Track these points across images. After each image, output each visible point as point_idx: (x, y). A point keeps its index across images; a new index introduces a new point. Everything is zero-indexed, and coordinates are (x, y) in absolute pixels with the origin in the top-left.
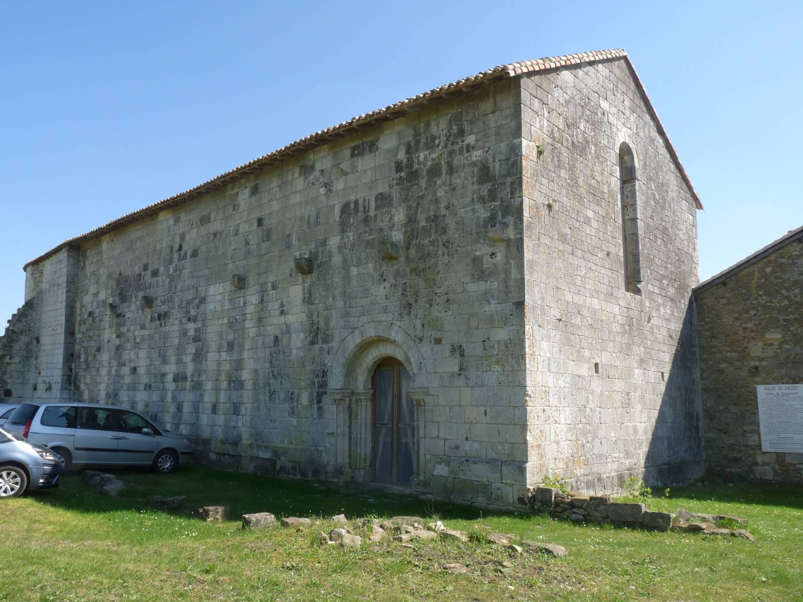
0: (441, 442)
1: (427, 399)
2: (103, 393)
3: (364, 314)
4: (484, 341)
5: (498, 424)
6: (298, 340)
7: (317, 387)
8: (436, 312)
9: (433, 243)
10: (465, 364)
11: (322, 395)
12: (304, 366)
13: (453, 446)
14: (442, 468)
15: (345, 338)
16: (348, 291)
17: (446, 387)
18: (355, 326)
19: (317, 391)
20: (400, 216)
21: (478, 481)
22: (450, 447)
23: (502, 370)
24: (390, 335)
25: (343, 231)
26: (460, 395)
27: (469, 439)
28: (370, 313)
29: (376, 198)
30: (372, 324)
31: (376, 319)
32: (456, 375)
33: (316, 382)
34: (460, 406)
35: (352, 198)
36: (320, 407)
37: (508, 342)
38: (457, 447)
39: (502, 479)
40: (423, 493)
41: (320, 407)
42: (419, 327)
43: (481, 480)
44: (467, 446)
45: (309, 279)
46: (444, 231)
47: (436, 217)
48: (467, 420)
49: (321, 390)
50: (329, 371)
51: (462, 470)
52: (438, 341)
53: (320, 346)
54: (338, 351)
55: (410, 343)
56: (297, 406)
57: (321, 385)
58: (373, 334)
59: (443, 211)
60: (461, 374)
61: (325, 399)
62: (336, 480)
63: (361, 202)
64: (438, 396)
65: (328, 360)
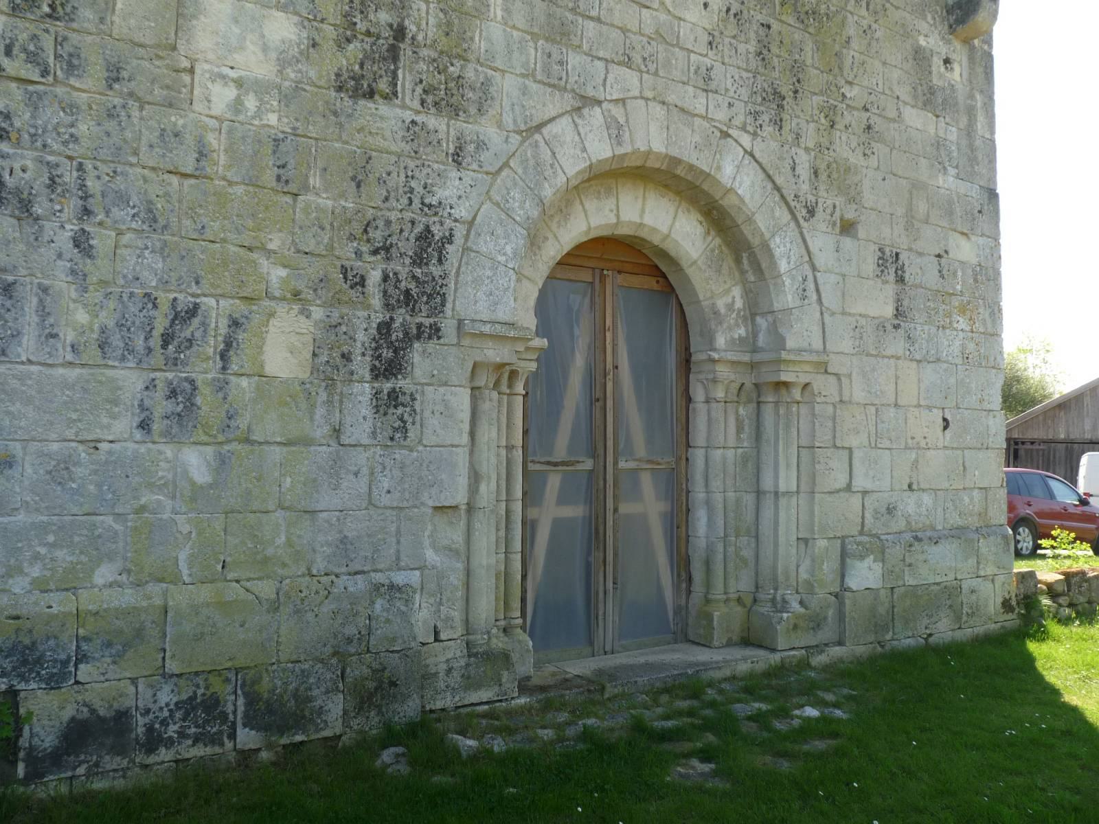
0: (856, 501)
1: (820, 383)
3: (628, 63)
4: (939, 256)
5: (963, 449)
7: (376, 301)
8: (845, 147)
10: (906, 303)
11: (408, 338)
12: (288, 184)
13: (883, 510)
14: (870, 569)
17: (868, 355)
18: (590, 92)
19: (378, 318)
21: (938, 584)
22: (876, 512)
23: (968, 328)
24: (719, 168)
26: (897, 378)
27: (915, 487)
28: (652, 68)
30: (658, 110)
31: (672, 98)
32: (889, 327)
33: (374, 277)
34: (896, 405)
36: (394, 395)
37: (978, 269)
38: (890, 510)
39: (978, 569)
40: (819, 648)
41: (394, 395)
42: (804, 171)
43: (945, 579)
44: (910, 505)
48: (910, 441)
49: (401, 316)
51: (910, 565)
52: (848, 228)
53: (408, 116)
54: (506, 165)
55: (777, 214)
56: (221, 387)
57: (407, 292)
58: (658, 146)
61: (420, 359)
62: (485, 695)
64: (850, 376)
65: (454, 191)
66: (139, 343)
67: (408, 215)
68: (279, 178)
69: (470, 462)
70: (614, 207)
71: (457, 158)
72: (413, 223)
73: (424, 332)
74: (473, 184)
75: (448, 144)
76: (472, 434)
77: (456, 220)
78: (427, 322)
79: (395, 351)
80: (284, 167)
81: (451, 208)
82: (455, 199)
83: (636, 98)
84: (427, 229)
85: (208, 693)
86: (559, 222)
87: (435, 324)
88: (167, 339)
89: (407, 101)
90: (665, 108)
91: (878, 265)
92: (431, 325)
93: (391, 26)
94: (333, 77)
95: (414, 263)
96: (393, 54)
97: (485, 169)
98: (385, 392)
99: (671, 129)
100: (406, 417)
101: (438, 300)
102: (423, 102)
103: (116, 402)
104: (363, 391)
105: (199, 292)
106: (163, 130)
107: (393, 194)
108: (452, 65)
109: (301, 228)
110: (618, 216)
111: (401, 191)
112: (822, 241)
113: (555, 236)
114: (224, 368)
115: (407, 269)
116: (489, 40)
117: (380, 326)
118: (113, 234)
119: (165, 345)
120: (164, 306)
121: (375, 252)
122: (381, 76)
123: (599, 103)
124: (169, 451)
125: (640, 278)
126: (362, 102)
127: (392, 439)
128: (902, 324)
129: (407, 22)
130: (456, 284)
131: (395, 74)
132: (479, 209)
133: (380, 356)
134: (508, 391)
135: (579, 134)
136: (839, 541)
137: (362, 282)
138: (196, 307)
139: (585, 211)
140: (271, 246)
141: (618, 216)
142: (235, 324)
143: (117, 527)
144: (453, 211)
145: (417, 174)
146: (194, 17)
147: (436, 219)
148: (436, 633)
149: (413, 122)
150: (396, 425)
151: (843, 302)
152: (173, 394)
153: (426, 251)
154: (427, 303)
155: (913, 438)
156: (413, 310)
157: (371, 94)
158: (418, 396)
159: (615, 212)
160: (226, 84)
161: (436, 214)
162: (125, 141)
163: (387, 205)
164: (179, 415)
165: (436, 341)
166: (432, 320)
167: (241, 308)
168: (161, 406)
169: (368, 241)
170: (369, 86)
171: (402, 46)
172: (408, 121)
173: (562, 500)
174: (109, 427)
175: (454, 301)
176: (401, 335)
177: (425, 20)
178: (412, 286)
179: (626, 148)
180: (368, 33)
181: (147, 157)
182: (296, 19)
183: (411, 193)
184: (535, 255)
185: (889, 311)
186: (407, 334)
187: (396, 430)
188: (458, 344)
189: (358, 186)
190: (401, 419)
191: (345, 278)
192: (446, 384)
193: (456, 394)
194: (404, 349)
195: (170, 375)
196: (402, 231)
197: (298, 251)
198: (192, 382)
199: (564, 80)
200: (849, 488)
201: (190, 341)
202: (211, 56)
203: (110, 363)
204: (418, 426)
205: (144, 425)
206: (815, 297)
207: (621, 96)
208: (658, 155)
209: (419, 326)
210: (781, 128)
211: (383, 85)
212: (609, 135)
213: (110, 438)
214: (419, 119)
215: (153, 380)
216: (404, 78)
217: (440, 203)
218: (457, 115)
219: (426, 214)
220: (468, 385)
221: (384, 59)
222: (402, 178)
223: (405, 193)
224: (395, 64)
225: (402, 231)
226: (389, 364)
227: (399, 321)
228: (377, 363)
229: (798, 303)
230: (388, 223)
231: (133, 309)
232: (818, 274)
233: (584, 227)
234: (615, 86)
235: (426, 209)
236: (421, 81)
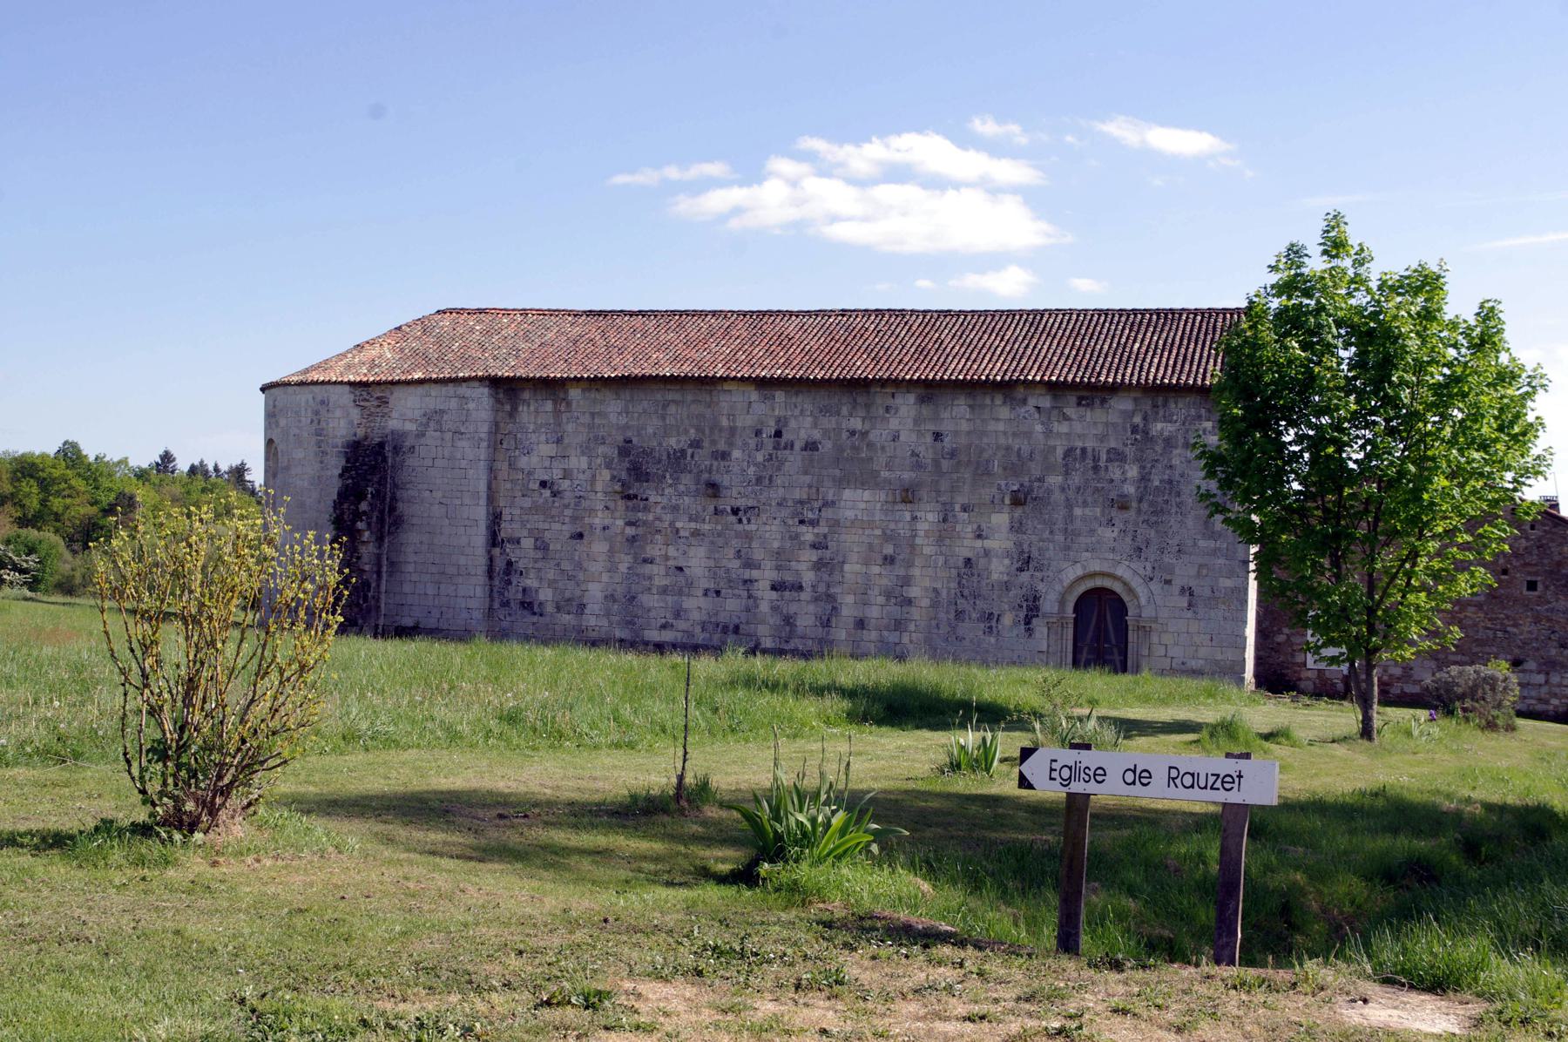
2: (595, 592)
6: (999, 569)
9: (1167, 502)
16: (1070, 528)
20: (1133, 472)
25: (1067, 473)
29: (1108, 452)
35: (1079, 444)
45: (1019, 511)
46: (1179, 494)
47: (1170, 482)
52: (1168, 582)
59: (1177, 477)
61: (1034, 621)
63: (1089, 450)
112: (1155, 586)
226: (1028, 621)
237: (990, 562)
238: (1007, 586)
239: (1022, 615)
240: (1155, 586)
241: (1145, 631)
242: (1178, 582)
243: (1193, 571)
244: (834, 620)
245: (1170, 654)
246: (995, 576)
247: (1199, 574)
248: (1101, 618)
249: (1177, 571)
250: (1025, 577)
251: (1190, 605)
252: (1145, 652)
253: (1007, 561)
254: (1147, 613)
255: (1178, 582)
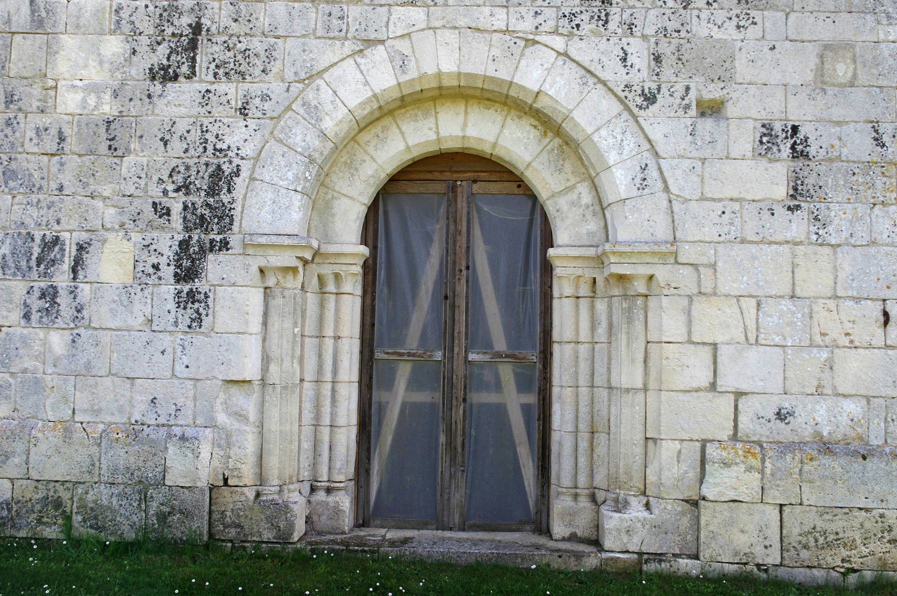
10: (811, 181)
11: (202, 251)
15: (326, 70)
33: (177, 209)
36: (192, 296)
50: (244, 174)
52: (711, 109)
53: (204, 87)
54: (289, 108)
56: (73, 292)
60: (798, 207)
61: (215, 267)
64: (713, 266)
66: (24, 264)
67: (204, 160)
68: (110, 147)
69: (263, 347)
70: (433, 126)
71: (243, 111)
72: (207, 165)
73: (215, 245)
74: (257, 128)
75: (236, 102)
76: (265, 324)
77: (242, 158)
78: (218, 238)
79: (192, 262)
80: (113, 139)
81: (238, 149)
82: (242, 142)
83: (423, 30)
84: (219, 167)
85: (56, 496)
86: (376, 146)
87: (225, 239)
88: (39, 262)
89: (203, 76)
90: (457, 31)
91: (761, 142)
92: (221, 241)
93: (190, 25)
94: (147, 71)
95: (208, 194)
96: (193, 45)
97: (268, 115)
98: (185, 292)
99: (463, 49)
100: (201, 310)
101: (227, 220)
102: (215, 74)
103: (11, 302)
104: (168, 289)
105: (59, 229)
106: (38, 128)
107: (191, 146)
108: (240, 42)
109: (125, 179)
110: (438, 133)
111: (198, 143)
112: (665, 125)
113: (372, 157)
114: (74, 279)
115: (202, 200)
116: (272, 16)
117: (181, 243)
118: (10, 197)
119: (38, 265)
120: (38, 240)
121: (177, 190)
122: (183, 63)
123: (382, 42)
124: (41, 334)
125: (500, 185)
126: (169, 85)
127: (190, 327)
128: (803, 204)
129: (203, 20)
130: (243, 207)
131: (194, 60)
132: (263, 147)
133: (181, 265)
134: (335, 291)
135: (362, 72)
136: (698, 444)
137: (168, 213)
138: (57, 238)
139: (402, 133)
140: (105, 194)
141: (438, 133)
142: (81, 248)
143: (11, 380)
144: (239, 152)
145: (210, 127)
146: (57, 53)
147: (226, 160)
148: (226, 480)
149: (208, 91)
150: (193, 317)
151: (702, 188)
152: (43, 296)
153: (217, 185)
154: (218, 223)
155: (823, 335)
156: (206, 230)
157: (175, 78)
158: (211, 295)
159: (434, 129)
160: (76, 92)
161: (226, 156)
162: (16, 138)
163: (187, 155)
164: (47, 309)
165: (225, 252)
166: (221, 236)
167: (84, 236)
168: (36, 304)
169: (173, 182)
170: (174, 71)
171: (199, 37)
172: (203, 91)
173: (414, 383)
174: (7, 317)
175: (241, 220)
176: (196, 249)
177: (218, 15)
178: (207, 212)
179: (412, 74)
180: (173, 35)
181: (29, 147)
182: (123, 37)
183: (206, 143)
184: (352, 175)
185: (781, 191)
186: (202, 247)
187: (193, 320)
188: (244, 254)
189: (165, 144)
190: (197, 312)
191: (156, 211)
192: (234, 285)
193: (242, 293)
194: (199, 260)
195: (43, 285)
196: (198, 172)
197: (124, 196)
198: (55, 288)
199: (344, 30)
200: (713, 386)
201: (53, 261)
202: (67, 76)
203: (7, 277)
204: (210, 317)
205: (27, 316)
206: (660, 184)
207: (406, 32)
208: (449, 74)
209: (212, 241)
210: (606, 22)
211: (185, 69)
212: (393, 67)
213: (8, 324)
214: (212, 88)
215: (32, 287)
216: (201, 60)
217: (229, 147)
218: (244, 79)
219: (218, 157)
220: (259, 284)
221: (186, 50)
222: (199, 133)
223: (201, 144)
224: (194, 52)
225: (198, 172)
226: (188, 270)
227: (196, 238)
228: (179, 271)
229: (635, 193)
230: (188, 168)
231: (20, 242)
232: (661, 161)
233: (401, 146)
234: (399, 24)
235: (218, 153)
236: (214, 60)
237: (51, 51)
238: (112, 138)
239: (167, 243)
240: (665, 125)
241: (622, 290)
242: (748, 109)
243: (799, 67)
244: (855, 445)
245: (729, 381)
246: (70, 101)
247: (821, 81)
248: (456, 266)
249: (742, 68)
250: (180, 100)
251: (797, 192)
252: (629, 375)
253: (114, 46)
254: (638, 224)
255: (748, 109)
